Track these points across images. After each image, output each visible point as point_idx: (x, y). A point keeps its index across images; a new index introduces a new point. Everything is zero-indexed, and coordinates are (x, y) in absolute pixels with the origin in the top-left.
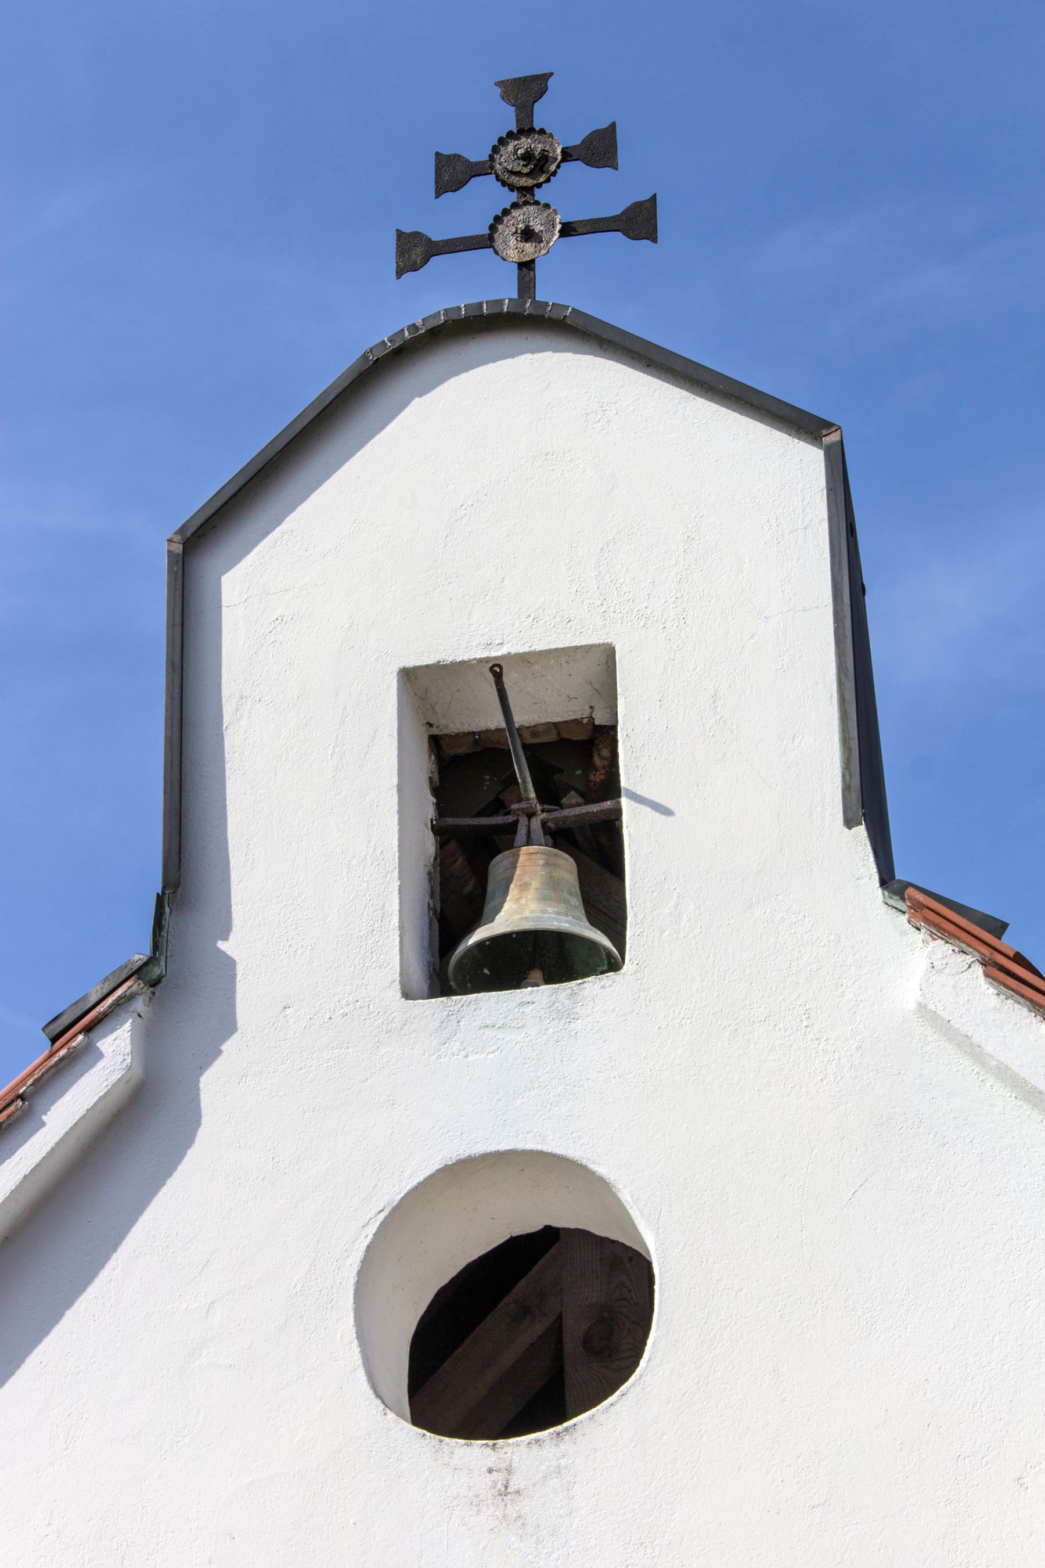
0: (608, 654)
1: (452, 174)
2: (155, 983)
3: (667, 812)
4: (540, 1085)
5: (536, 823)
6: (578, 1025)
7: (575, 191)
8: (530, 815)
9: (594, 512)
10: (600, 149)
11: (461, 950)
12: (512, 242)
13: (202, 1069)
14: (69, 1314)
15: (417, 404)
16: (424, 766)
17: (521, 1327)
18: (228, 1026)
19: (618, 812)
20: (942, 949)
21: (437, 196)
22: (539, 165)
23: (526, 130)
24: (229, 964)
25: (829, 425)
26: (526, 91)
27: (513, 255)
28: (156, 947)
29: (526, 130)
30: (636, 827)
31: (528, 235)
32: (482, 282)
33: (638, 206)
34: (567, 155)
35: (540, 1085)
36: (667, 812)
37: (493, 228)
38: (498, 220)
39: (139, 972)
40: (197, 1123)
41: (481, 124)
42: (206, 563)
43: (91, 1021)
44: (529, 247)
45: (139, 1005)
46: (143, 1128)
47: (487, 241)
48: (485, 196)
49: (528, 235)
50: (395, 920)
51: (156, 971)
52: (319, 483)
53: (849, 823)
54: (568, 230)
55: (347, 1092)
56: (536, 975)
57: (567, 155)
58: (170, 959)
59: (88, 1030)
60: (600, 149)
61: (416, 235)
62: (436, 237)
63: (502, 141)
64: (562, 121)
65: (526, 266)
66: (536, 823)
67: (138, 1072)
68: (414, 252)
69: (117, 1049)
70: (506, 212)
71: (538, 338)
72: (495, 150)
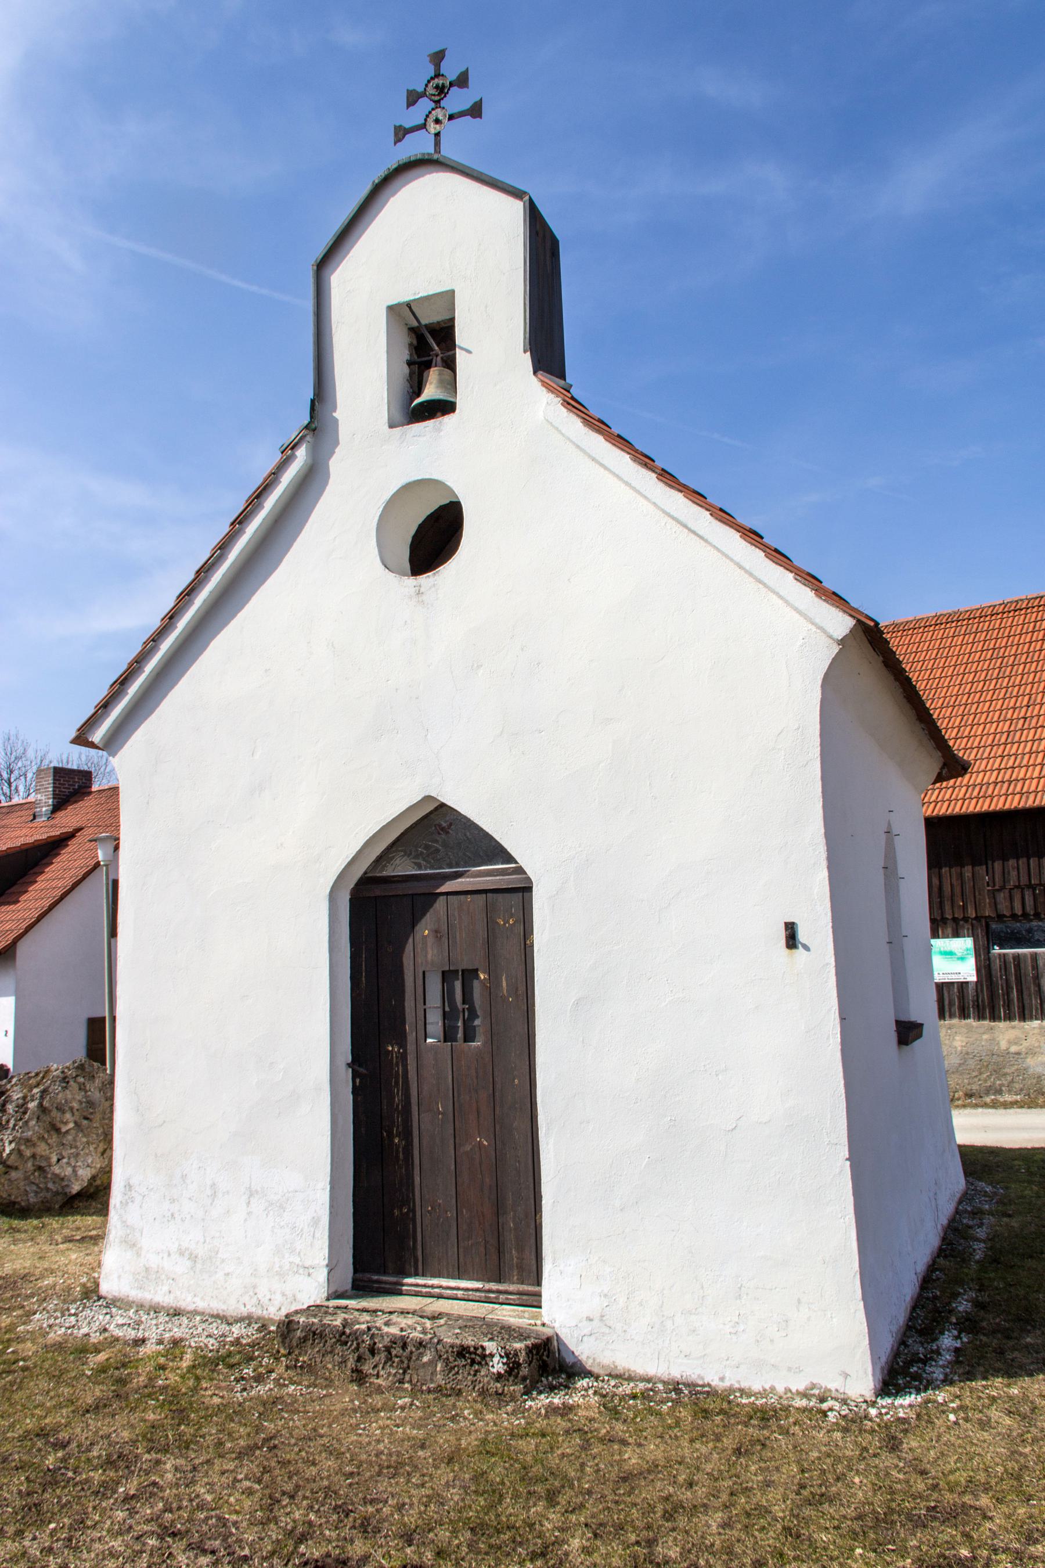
0: (453, 292)
1: (413, 98)
2: (314, 430)
3: (470, 352)
4: (439, 455)
5: (439, 358)
6: (442, 433)
7: (457, 100)
8: (437, 356)
9: (450, 239)
10: (462, 81)
11: (419, 408)
12: (432, 125)
13: (329, 459)
14: (295, 544)
15: (392, 200)
16: (404, 340)
17: (434, 537)
18: (337, 443)
19: (455, 354)
20: (551, 396)
21: (408, 107)
22: (442, 90)
23: (437, 75)
24: (336, 421)
25: (525, 193)
26: (438, 57)
27: (433, 131)
28: (311, 417)
29: (437, 75)
30: (460, 357)
31: (437, 121)
32: (419, 145)
33: (476, 103)
34: (451, 84)
35: (439, 455)
36: (470, 352)
37: (426, 120)
38: (427, 116)
39: (307, 427)
40: (328, 477)
41: (420, 77)
42: (326, 272)
43: (294, 446)
44: (438, 126)
45: (308, 438)
46: (312, 480)
47: (424, 126)
48: (425, 105)
49: (437, 121)
50: (386, 401)
51: (313, 426)
52: (360, 236)
53: (525, 352)
54: (451, 118)
55: (375, 461)
56: (439, 414)
57: (451, 84)
58: (318, 422)
59: (292, 448)
60: (462, 81)
61: (400, 126)
62: (407, 126)
63: (429, 82)
64: (450, 71)
65: (437, 135)
66: (439, 358)
67: (310, 462)
68: (401, 133)
69: (302, 454)
70: (430, 113)
71: (431, 168)
72: (426, 86)
